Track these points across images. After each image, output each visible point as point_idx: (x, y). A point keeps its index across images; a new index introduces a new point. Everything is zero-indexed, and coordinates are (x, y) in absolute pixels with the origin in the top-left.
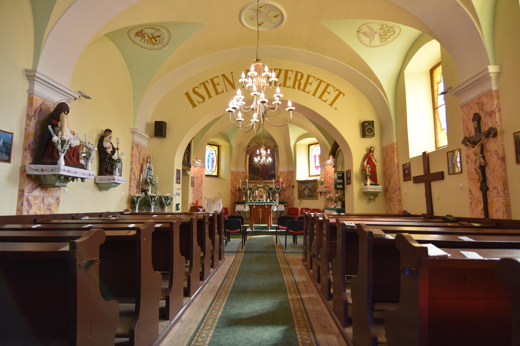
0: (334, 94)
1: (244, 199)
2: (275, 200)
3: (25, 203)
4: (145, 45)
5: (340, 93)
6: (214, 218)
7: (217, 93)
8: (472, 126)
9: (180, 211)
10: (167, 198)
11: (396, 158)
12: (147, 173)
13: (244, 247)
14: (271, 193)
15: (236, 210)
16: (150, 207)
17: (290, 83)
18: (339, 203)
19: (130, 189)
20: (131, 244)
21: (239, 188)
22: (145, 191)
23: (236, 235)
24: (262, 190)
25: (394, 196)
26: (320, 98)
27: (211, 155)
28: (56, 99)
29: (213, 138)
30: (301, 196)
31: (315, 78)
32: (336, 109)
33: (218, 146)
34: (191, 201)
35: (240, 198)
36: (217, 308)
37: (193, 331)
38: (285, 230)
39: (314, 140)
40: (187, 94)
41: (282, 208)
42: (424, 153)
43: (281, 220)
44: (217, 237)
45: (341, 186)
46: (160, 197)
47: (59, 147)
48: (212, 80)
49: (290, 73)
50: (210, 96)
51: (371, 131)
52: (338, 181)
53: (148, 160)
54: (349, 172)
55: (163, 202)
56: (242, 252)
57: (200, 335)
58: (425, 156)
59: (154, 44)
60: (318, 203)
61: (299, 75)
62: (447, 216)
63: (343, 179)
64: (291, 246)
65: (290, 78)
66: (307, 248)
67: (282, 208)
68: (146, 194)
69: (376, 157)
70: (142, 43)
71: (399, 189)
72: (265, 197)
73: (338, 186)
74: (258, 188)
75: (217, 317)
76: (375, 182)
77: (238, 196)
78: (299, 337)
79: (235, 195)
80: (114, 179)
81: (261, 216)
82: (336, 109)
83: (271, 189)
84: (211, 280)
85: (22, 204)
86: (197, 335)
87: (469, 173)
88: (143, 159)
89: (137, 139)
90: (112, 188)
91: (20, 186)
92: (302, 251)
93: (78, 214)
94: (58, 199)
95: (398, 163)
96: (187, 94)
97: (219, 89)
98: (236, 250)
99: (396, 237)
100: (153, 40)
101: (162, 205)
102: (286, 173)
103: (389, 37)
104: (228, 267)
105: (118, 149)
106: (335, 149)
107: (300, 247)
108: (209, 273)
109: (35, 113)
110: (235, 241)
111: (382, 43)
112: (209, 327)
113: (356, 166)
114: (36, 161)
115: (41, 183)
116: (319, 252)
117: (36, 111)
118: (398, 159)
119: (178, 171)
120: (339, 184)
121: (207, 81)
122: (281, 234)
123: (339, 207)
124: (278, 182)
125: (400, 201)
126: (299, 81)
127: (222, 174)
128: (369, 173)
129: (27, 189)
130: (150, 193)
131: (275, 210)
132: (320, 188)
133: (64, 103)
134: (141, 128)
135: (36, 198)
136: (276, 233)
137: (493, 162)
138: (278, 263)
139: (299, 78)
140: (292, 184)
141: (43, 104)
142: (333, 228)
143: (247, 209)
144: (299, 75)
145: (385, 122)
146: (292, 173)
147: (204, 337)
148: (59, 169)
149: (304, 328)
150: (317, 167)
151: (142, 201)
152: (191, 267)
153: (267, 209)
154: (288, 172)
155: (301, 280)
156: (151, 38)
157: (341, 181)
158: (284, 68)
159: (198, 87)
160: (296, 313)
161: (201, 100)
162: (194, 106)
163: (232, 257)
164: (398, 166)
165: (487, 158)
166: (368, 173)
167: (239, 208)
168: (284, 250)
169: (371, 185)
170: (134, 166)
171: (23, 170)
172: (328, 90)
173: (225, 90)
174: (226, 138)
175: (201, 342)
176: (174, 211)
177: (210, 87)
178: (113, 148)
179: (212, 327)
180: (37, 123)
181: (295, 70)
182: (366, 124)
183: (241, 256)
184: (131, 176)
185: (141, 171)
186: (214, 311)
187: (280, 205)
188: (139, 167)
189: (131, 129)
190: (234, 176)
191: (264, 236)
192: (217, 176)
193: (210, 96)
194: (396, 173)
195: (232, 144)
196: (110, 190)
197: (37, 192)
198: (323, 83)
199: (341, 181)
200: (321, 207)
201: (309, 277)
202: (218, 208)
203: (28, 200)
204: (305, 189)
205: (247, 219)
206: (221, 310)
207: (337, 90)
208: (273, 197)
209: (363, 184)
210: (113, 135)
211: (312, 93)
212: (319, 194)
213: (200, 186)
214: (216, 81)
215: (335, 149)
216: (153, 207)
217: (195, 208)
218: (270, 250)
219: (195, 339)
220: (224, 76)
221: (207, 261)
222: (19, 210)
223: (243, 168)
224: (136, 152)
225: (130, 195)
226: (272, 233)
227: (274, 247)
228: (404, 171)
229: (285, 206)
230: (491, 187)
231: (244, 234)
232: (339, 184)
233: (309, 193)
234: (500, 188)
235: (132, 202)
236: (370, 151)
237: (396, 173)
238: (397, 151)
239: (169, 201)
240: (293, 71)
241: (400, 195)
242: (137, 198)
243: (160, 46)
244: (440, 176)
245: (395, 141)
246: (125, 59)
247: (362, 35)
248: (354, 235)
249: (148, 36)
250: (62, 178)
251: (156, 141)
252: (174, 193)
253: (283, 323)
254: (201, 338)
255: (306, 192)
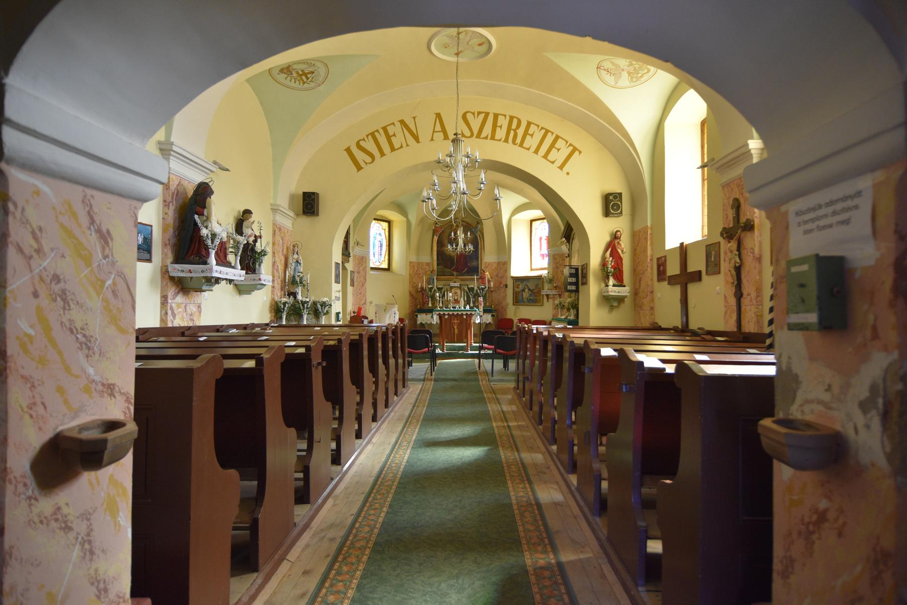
0: (566, 151)
1: (430, 305)
2: (478, 307)
3: (169, 312)
4: (292, 84)
5: (575, 149)
6: (341, 351)
7: (393, 149)
8: (731, 213)
9: (340, 323)
10: (324, 304)
11: (649, 248)
12: (295, 269)
13: (434, 373)
14: (472, 296)
15: (419, 322)
16: (301, 316)
17: (501, 133)
18: (573, 312)
19: (273, 292)
20: (254, 378)
21: (422, 288)
22: (294, 295)
23: (421, 359)
24: (459, 291)
25: (645, 301)
26: (545, 157)
27: (378, 236)
28: (197, 177)
29: (385, 208)
30: (518, 301)
31: (538, 126)
32: (568, 174)
33: (389, 222)
34: (350, 308)
35: (424, 303)
36: (377, 506)
37: (388, 452)
38: (491, 352)
39: (538, 213)
40: (348, 150)
41: (488, 318)
42: (682, 244)
43: (486, 335)
44: (392, 361)
45: (574, 288)
46: (315, 303)
47: (209, 242)
48: (385, 129)
49: (500, 118)
50: (382, 154)
51: (618, 207)
52: (570, 280)
53: (294, 249)
54: (585, 267)
55: (317, 310)
56: (431, 380)
57: (344, 559)
58: (683, 250)
59: (304, 83)
60: (545, 311)
61: (515, 122)
62: (699, 329)
63: (579, 276)
64: (500, 373)
65: (501, 127)
66: (522, 378)
67: (488, 318)
68: (295, 297)
69: (623, 245)
70: (287, 82)
71: (652, 292)
72: (462, 303)
73: (569, 287)
74: (452, 288)
75: (376, 522)
76: (620, 283)
77: (420, 301)
78: (512, 493)
79: (416, 299)
80: (260, 279)
81: (456, 331)
82: (568, 174)
83: (471, 290)
84: (396, 409)
85: (166, 313)
86: (340, 559)
87: (725, 274)
88: (287, 248)
89: (280, 220)
90: (256, 291)
91: (162, 291)
92: (513, 378)
93: (222, 326)
94: (199, 307)
95: (652, 256)
96: (348, 150)
97: (396, 142)
98: (422, 377)
99: (677, 369)
100: (304, 77)
101: (316, 314)
102: (495, 265)
103: (642, 76)
104: (415, 396)
105: (260, 237)
106: (568, 231)
107: (512, 374)
108: (393, 402)
109: (172, 198)
110: (419, 368)
111: (633, 84)
112: (363, 543)
113: (595, 261)
114: (178, 260)
115: (184, 286)
116: (542, 385)
117: (173, 194)
118: (652, 250)
119: (337, 264)
120: (571, 284)
121: (377, 131)
122: (486, 356)
123: (572, 317)
124: (482, 279)
125: (652, 308)
126: (515, 130)
127: (395, 265)
128: (613, 270)
129: (170, 295)
130: (300, 297)
131: (478, 321)
132: (546, 290)
133: (207, 184)
134: (283, 202)
135: (179, 306)
136: (479, 356)
137: (749, 262)
138: (482, 392)
139: (514, 127)
140: (504, 283)
141: (179, 185)
142: (560, 346)
143: (435, 320)
144: (515, 122)
145: (636, 197)
146: (504, 265)
147: (352, 564)
148: (211, 270)
149: (539, 545)
150: (543, 256)
151: (291, 309)
152: (340, 419)
153: (465, 321)
154: (499, 263)
155: (510, 409)
156: (301, 75)
157: (574, 280)
158: (492, 111)
159: (364, 140)
160: (509, 467)
161: (369, 159)
162: (359, 168)
163: (419, 386)
164: (651, 260)
165: (744, 257)
166: (610, 269)
167: (422, 318)
168: (490, 377)
169: (614, 286)
170: (277, 259)
171: (165, 272)
172: (557, 146)
173: (404, 145)
174: (401, 209)
175: (346, 573)
176: (333, 322)
177: (382, 140)
178: (255, 236)
179: (367, 543)
180: (175, 210)
181: (508, 114)
182: (611, 198)
183: (430, 385)
184: (273, 273)
185: (286, 266)
186: (372, 512)
187: (486, 315)
188: (283, 259)
189: (271, 205)
190: (415, 269)
191: (461, 359)
192: (388, 269)
193: (382, 154)
194: (649, 270)
195: (410, 217)
196: (253, 293)
197: (180, 299)
198: (550, 134)
199: (574, 280)
200: (547, 316)
201: (520, 407)
202: (392, 318)
203: (172, 309)
204: (524, 290)
205: (436, 335)
206: (385, 509)
207: (571, 145)
208: (474, 303)
209: (603, 285)
210: (254, 217)
211: (533, 149)
212: (545, 297)
213: (363, 285)
214: (391, 130)
215: (568, 231)
216: (305, 317)
217: (358, 318)
218: (472, 375)
219: (336, 567)
220: (402, 122)
221: (367, 411)
222: (163, 320)
223: (429, 258)
224: (278, 238)
225: (273, 299)
226: (473, 356)
227: (475, 373)
228: (659, 266)
229: (493, 316)
230: (745, 292)
231: (434, 357)
232: (571, 284)
233: (530, 295)
234: (753, 295)
235: (277, 310)
236: (615, 237)
237: (649, 270)
238: (652, 239)
239: (327, 308)
240: (505, 116)
241: (653, 300)
242: (284, 304)
243: (312, 85)
244: (697, 277)
245: (649, 224)
246: (261, 103)
247: (603, 73)
248: (582, 355)
249: (297, 72)
250: (213, 280)
251: (306, 220)
252: (333, 298)
253: (485, 444)
254: (346, 565)
255: (526, 294)
